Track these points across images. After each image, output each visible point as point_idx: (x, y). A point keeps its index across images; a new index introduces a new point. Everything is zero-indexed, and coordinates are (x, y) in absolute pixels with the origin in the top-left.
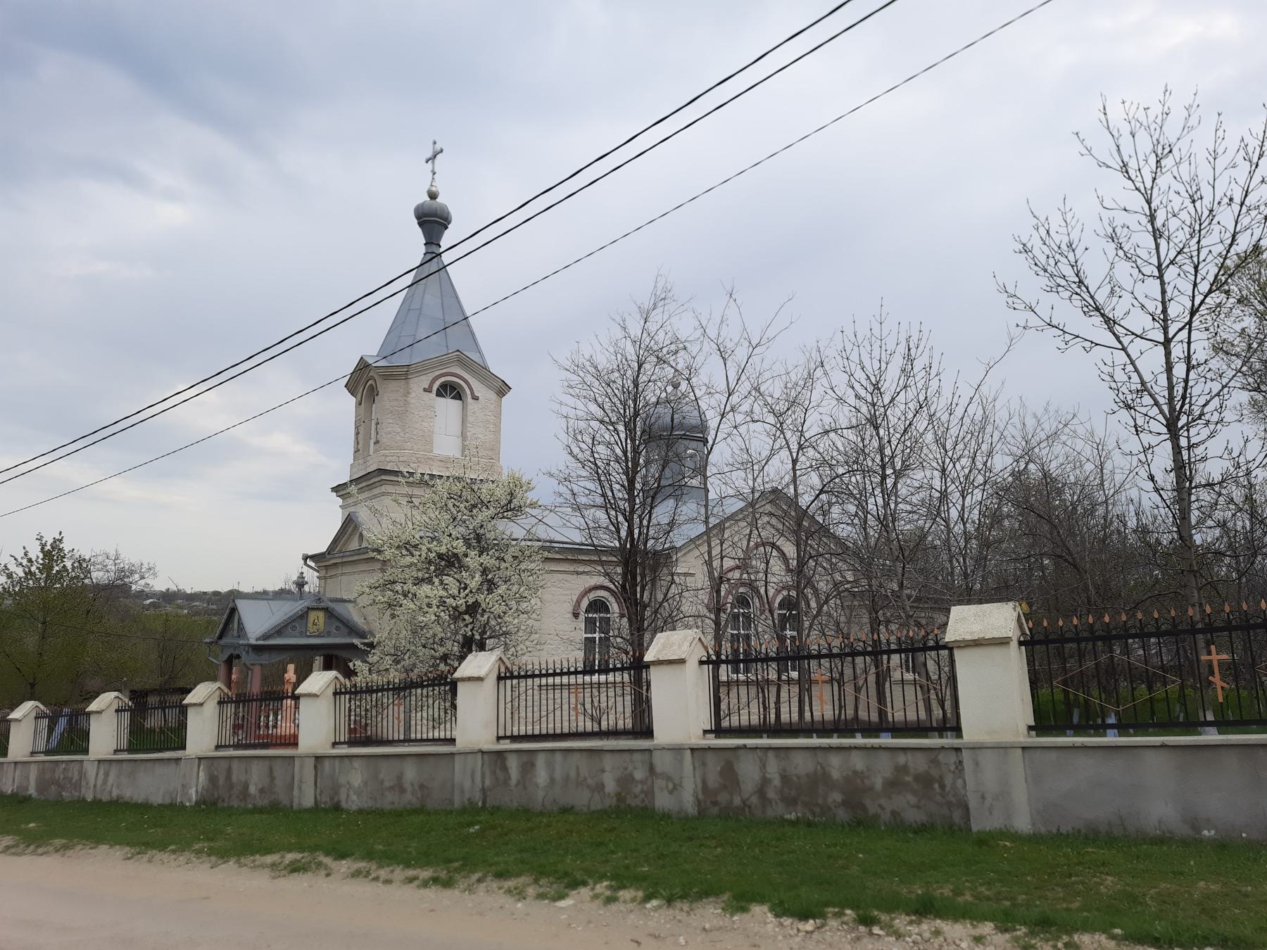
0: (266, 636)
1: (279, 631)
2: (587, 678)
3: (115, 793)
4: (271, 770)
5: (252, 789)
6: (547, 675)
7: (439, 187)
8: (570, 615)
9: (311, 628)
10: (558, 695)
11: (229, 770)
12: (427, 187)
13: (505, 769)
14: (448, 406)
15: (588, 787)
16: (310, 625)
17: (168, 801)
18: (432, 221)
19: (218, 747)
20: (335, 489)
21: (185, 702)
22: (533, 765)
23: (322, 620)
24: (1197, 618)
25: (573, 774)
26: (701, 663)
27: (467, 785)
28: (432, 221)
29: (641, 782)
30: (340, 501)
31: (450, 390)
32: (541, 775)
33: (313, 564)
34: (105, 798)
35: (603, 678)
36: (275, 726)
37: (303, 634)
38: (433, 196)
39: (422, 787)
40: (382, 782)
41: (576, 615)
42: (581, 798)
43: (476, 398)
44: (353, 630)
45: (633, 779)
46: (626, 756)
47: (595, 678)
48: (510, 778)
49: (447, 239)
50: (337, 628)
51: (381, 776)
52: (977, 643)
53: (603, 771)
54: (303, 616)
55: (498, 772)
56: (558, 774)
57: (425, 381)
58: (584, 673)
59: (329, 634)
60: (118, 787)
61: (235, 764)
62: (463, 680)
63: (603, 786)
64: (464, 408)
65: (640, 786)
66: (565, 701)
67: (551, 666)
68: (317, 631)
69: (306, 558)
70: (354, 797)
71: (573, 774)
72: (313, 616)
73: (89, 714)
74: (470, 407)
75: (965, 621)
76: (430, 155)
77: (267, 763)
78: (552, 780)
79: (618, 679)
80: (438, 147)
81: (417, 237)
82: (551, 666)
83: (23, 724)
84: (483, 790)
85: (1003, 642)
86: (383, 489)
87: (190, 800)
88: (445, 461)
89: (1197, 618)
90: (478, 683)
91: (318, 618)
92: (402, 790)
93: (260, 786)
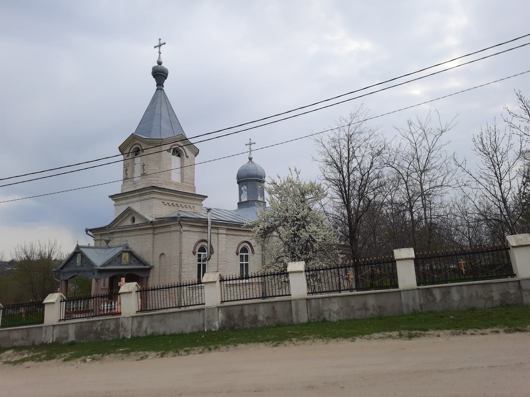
0: (104, 265)
1: (109, 263)
2: (241, 281)
3: (149, 331)
4: (273, 308)
5: (261, 318)
6: (230, 280)
7: (163, 60)
8: (235, 254)
9: (123, 261)
10: (232, 289)
11: (242, 311)
12: (157, 59)
13: (433, 295)
14: (176, 161)
15: (484, 298)
16: (123, 259)
17: (181, 332)
18: (160, 75)
19: (222, 302)
20: (110, 197)
21: (44, 302)
22: (449, 292)
23: (128, 257)
24: (453, 252)
25: (474, 294)
26: (136, 292)
27: (411, 303)
28: (160, 75)
29: (514, 294)
30: (114, 202)
31: (177, 152)
32: (455, 296)
33: (91, 234)
34: (141, 335)
35: (247, 281)
36: (115, 309)
37: (120, 264)
38: (160, 63)
39: (379, 307)
40: (353, 307)
41: (237, 254)
42: (480, 304)
43: (187, 157)
44: (139, 261)
45: (509, 293)
46: (505, 285)
47: (244, 281)
48: (436, 299)
49: (166, 83)
50: (134, 261)
51: (352, 304)
52: (402, 259)
53: (492, 291)
54: (119, 256)
55: (428, 297)
56: (465, 295)
57: (168, 147)
58: (239, 279)
59: (130, 264)
60: (152, 328)
61: (246, 308)
62: (291, 272)
63: (492, 297)
64: (182, 161)
65: (513, 296)
66: (235, 291)
67: (167, 285)
68: (126, 263)
69: (87, 231)
70: (335, 315)
71: (474, 294)
72: (124, 255)
73: (120, 294)
74: (185, 161)
75: (400, 253)
76: (157, 44)
77: (270, 305)
78: (462, 298)
79: (260, 281)
80: (162, 42)
81: (153, 82)
82: (167, 285)
83: (55, 305)
84: (420, 305)
85: (302, 272)
86: (152, 196)
87: (215, 328)
88: (176, 184)
89: (453, 252)
90: (129, 294)
91: (126, 256)
92: (367, 309)
93: (266, 316)
